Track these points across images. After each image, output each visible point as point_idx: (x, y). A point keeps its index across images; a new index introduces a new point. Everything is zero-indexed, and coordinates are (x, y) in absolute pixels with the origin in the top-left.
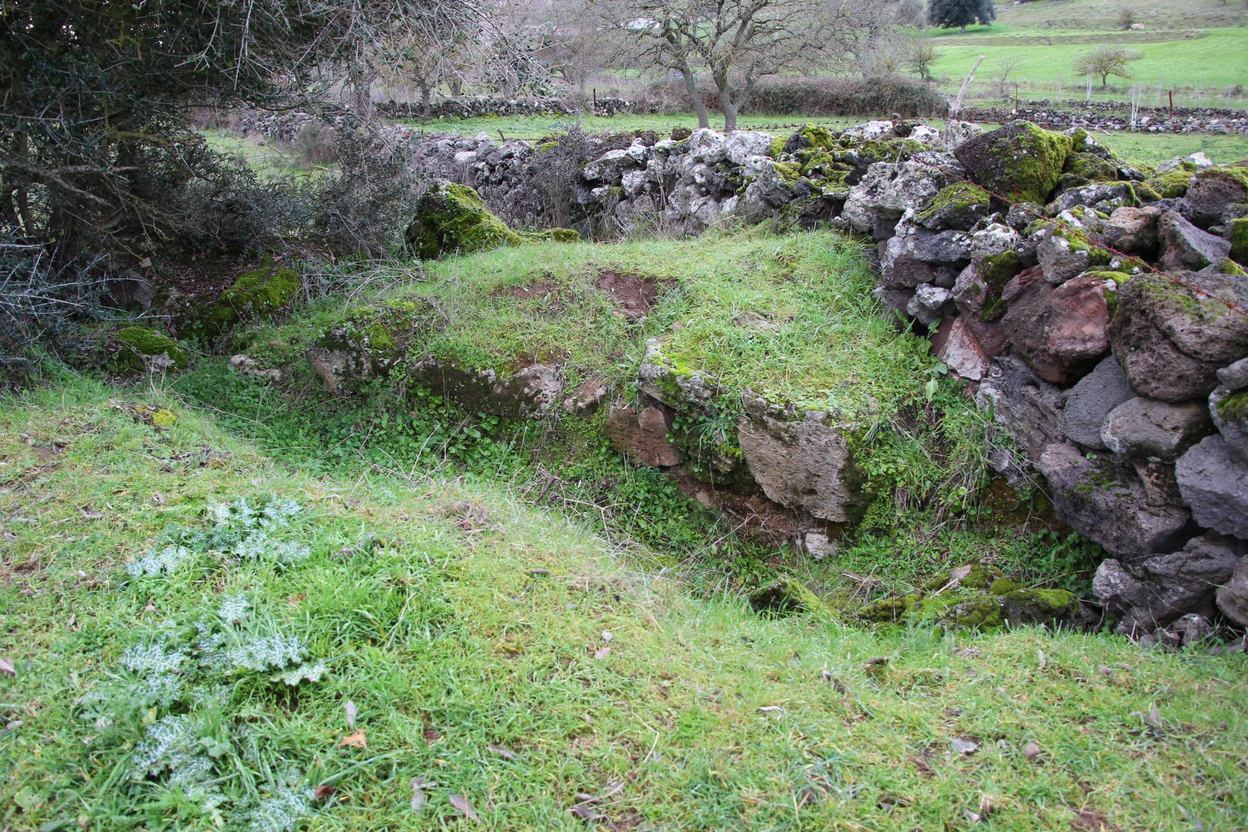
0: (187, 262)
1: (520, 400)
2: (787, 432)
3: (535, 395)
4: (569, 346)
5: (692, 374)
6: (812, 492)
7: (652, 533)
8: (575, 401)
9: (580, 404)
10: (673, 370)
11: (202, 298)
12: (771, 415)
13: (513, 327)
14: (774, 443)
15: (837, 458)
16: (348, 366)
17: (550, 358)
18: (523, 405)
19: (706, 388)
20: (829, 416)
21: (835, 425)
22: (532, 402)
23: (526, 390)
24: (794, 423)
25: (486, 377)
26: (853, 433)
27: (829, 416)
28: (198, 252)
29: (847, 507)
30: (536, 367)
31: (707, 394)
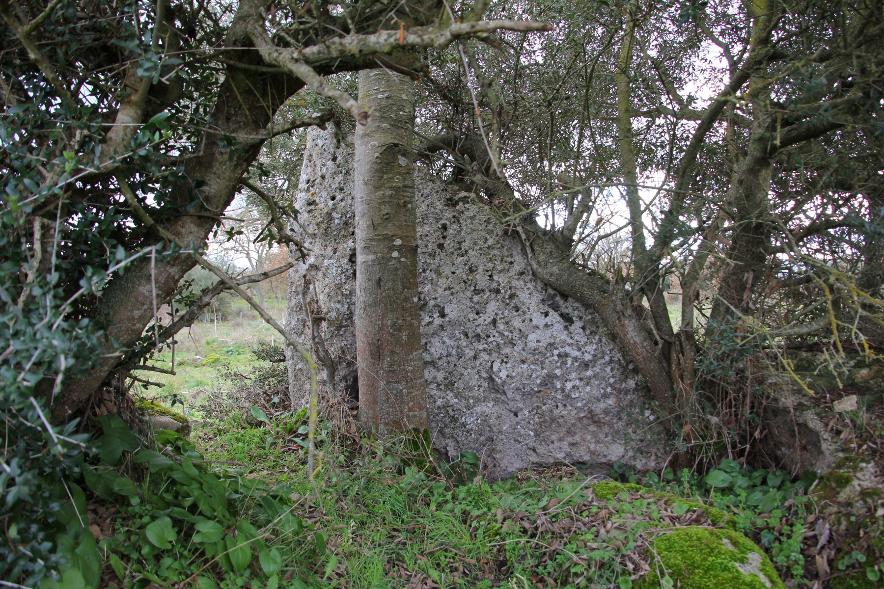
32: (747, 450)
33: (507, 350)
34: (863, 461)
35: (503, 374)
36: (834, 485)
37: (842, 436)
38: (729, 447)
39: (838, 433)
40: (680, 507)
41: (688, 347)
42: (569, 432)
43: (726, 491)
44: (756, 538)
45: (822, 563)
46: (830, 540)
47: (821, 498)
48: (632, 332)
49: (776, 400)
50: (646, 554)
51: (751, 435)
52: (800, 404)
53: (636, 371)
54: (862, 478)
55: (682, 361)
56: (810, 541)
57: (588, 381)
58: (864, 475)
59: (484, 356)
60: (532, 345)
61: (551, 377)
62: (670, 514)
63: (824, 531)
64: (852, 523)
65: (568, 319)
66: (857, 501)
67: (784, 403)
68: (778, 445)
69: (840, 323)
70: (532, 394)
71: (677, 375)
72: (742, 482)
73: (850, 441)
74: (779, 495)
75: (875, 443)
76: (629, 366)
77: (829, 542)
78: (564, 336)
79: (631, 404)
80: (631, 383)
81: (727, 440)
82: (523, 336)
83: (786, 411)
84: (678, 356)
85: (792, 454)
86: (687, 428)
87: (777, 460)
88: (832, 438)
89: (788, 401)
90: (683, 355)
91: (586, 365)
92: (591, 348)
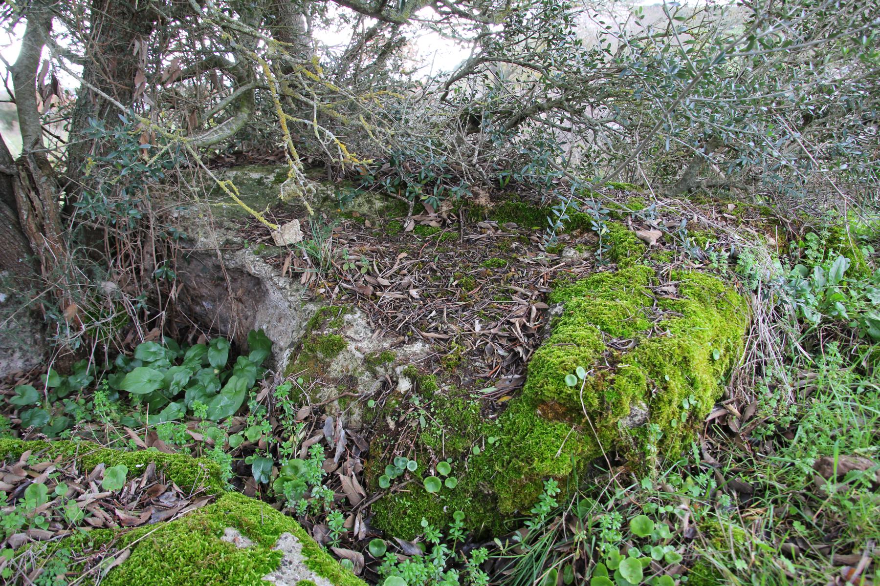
32: (164, 318)
34: (345, 311)
36: (320, 355)
37: (303, 279)
38: (136, 319)
39: (297, 276)
41: (43, 179)
46: (350, 444)
47: (307, 379)
49: (192, 241)
51: (165, 296)
52: (228, 242)
54: (357, 337)
55: (37, 203)
58: (356, 332)
62: (97, 495)
64: (370, 410)
66: (361, 374)
67: (205, 244)
69: (290, 118)
71: (33, 227)
73: (316, 285)
75: (348, 282)
77: (349, 447)
83: (209, 254)
84: (28, 196)
85: (229, 311)
86: (71, 311)
88: (291, 284)
89: (210, 240)
90: (37, 193)
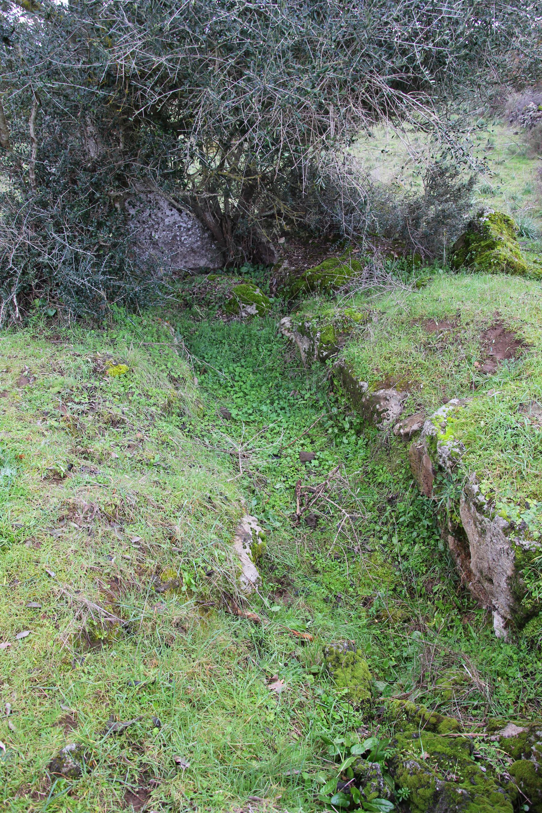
0: (305, 244)
1: (373, 412)
2: (480, 524)
3: (382, 412)
4: (424, 381)
5: (447, 442)
6: (491, 581)
7: (396, 550)
8: (401, 427)
9: (402, 431)
10: (441, 435)
11: (297, 272)
12: (475, 504)
13: (399, 354)
14: (473, 526)
15: (507, 566)
16: (309, 349)
17: (406, 387)
18: (375, 416)
19: (450, 459)
20: (512, 526)
21: (512, 537)
22: (380, 415)
23: (378, 406)
24: (486, 519)
25: (362, 387)
26: (525, 551)
27: (512, 526)
28: (315, 238)
29: (513, 611)
30: (391, 392)
31: (449, 463)
33: (156, 226)
35: (157, 237)
40: (236, 280)
42: (185, 257)
43: (247, 273)
44: (257, 285)
45: (274, 289)
48: (209, 218)
50: (231, 293)
53: (208, 229)
56: (271, 284)
57: (190, 236)
59: (147, 230)
60: (167, 223)
61: (176, 236)
63: (275, 281)
65: (180, 211)
68: (261, 254)
70: (168, 243)
72: (252, 269)
74: (262, 272)
76: (205, 227)
78: (179, 219)
79: (207, 243)
80: (206, 235)
81: (245, 255)
82: (163, 220)
87: (261, 260)
89: (264, 240)
91: (189, 230)
92: (190, 223)
